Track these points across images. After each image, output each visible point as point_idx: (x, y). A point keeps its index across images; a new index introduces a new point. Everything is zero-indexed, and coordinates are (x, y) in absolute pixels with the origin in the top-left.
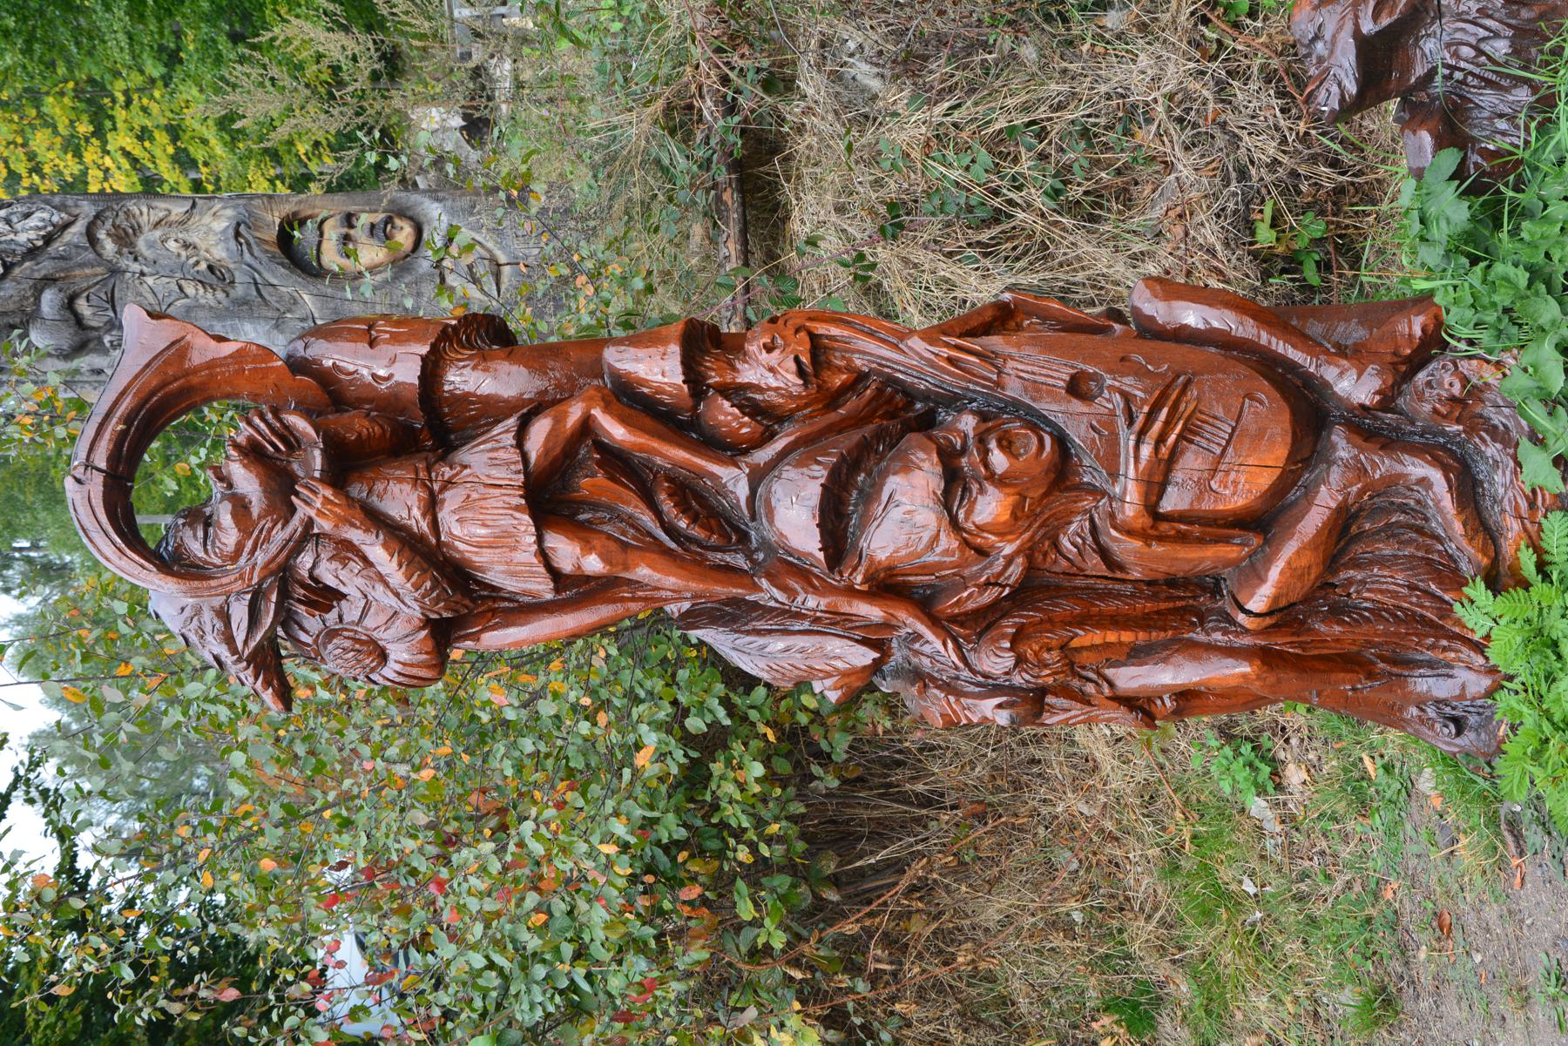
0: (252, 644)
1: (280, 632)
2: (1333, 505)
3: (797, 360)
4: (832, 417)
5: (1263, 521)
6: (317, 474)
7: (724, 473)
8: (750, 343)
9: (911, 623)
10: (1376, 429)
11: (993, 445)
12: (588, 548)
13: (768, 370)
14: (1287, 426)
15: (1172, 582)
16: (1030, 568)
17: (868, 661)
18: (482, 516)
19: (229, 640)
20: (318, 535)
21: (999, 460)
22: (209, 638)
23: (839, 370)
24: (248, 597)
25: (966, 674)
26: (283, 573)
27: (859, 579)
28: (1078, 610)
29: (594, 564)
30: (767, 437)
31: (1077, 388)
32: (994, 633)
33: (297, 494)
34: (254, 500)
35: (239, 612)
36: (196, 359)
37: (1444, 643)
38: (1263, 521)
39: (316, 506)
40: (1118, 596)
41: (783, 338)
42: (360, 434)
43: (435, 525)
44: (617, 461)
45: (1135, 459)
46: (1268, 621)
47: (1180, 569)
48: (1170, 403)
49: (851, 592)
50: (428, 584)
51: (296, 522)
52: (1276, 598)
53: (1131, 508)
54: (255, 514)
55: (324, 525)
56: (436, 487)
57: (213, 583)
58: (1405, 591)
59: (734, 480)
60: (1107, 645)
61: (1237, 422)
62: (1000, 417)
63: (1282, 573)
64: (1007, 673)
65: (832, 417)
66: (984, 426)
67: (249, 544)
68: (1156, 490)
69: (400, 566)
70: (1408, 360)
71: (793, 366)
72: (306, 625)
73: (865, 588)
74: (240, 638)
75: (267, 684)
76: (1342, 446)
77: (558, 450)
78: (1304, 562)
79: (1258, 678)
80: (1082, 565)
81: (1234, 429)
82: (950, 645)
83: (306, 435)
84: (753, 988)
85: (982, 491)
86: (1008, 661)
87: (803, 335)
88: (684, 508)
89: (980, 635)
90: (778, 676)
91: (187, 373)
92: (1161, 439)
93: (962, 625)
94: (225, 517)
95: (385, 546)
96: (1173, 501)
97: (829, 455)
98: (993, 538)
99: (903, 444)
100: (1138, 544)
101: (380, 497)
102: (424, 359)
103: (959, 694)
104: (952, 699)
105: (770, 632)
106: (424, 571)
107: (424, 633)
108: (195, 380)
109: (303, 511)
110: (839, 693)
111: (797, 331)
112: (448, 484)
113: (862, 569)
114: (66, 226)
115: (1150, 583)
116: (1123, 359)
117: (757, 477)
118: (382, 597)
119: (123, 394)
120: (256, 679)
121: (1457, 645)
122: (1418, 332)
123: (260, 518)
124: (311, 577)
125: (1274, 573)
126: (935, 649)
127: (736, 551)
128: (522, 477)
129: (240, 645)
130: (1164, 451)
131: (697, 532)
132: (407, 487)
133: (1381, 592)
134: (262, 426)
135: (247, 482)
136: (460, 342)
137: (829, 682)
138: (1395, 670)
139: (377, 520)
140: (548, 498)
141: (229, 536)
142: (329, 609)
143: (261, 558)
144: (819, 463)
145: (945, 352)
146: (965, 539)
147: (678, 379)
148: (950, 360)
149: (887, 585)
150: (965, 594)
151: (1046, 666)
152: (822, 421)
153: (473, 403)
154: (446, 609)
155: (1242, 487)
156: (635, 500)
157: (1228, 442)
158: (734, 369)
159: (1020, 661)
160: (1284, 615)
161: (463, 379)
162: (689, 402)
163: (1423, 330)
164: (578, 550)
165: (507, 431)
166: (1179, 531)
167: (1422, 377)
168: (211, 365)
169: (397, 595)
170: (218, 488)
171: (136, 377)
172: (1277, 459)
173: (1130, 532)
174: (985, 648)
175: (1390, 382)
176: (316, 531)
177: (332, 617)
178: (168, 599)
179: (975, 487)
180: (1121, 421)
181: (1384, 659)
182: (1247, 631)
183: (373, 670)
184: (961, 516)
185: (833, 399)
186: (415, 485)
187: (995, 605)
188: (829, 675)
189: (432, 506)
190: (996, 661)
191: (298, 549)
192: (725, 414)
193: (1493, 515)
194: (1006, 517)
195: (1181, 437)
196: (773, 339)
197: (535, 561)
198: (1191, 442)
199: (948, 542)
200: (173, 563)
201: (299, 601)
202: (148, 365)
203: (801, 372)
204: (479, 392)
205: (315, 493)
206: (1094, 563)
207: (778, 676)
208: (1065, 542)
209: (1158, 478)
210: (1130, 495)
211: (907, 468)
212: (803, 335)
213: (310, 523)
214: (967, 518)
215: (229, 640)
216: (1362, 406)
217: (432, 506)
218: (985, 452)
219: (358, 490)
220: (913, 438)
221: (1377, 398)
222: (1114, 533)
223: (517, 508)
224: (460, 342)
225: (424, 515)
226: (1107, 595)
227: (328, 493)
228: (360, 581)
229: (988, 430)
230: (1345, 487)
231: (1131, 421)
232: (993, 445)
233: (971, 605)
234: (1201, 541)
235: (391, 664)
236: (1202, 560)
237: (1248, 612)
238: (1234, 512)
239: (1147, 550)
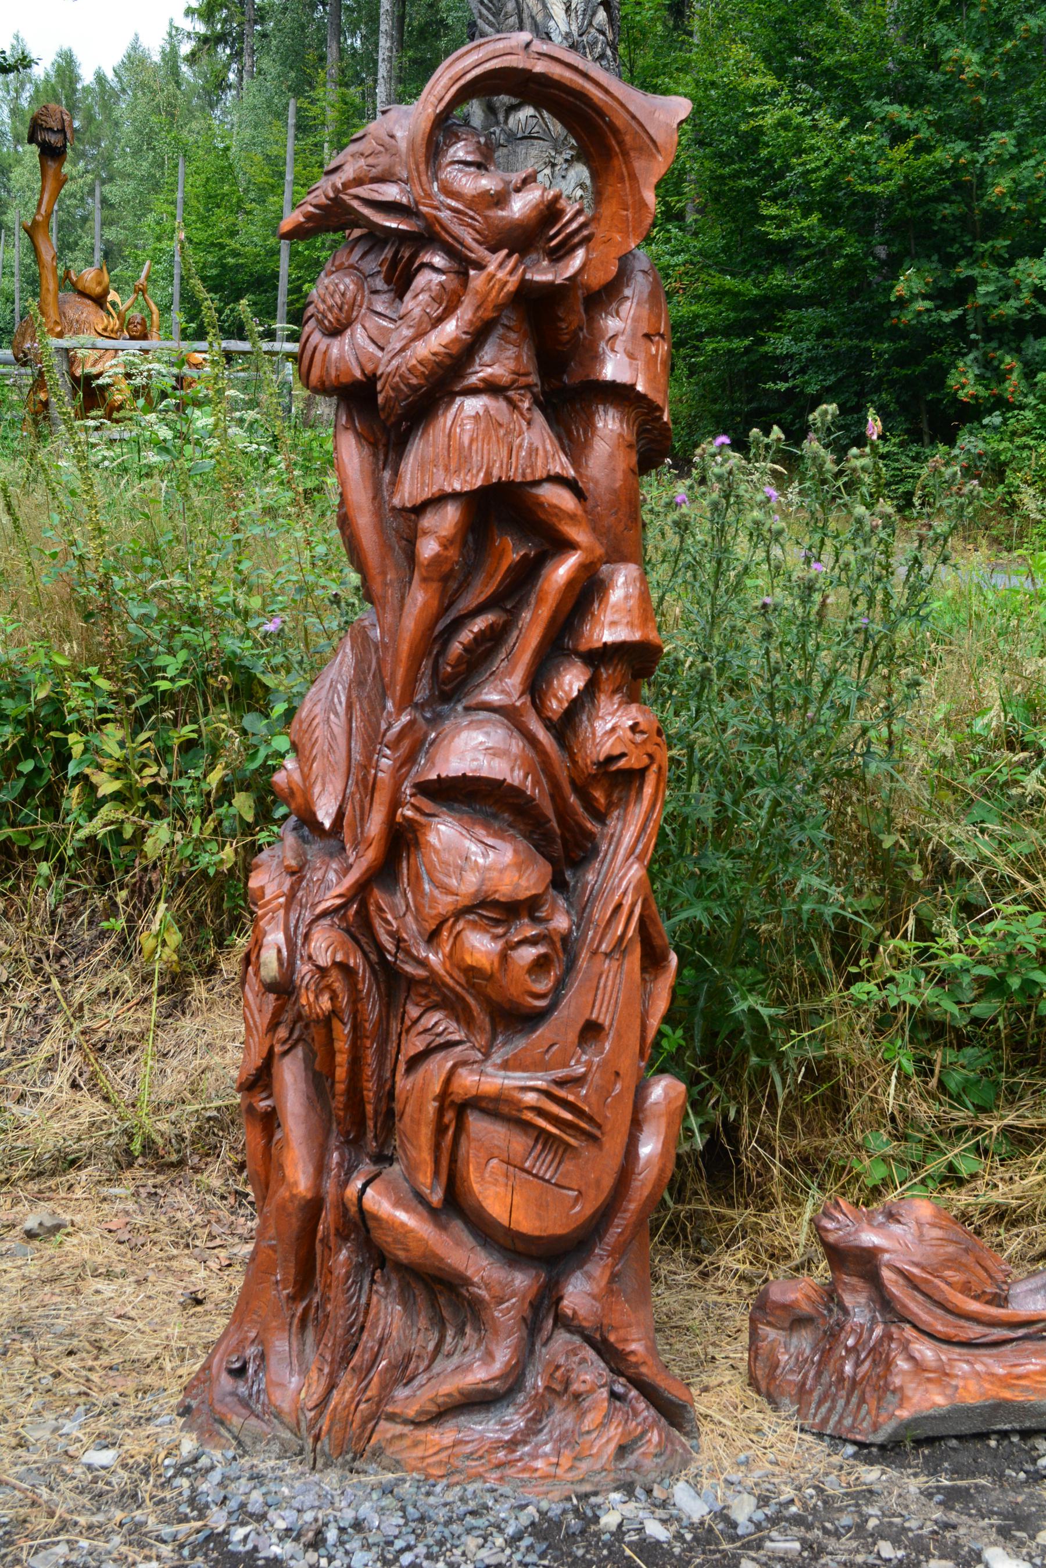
0: (355, 204)
1: (357, 233)
2: (469, 1273)
3: (623, 755)
4: (567, 788)
5: (455, 1205)
6: (528, 276)
7: (514, 681)
8: (639, 710)
9: (362, 861)
10: (544, 1311)
11: (541, 950)
12: (446, 544)
13: (612, 726)
14: (551, 1231)
15: (390, 1114)
16: (412, 982)
18: (478, 438)
19: (359, 182)
20: (466, 274)
21: (529, 953)
22: (362, 162)
23: (609, 796)
24: (405, 200)
25: (308, 916)
26: (430, 236)
27: (409, 813)
28: (369, 1026)
29: (428, 548)
30: (549, 725)
31: (591, 1031)
32: (351, 944)
33: (509, 256)
34: (501, 213)
35: (391, 192)
36: (639, 164)
37: (326, 1370)
38: (455, 1205)
39: (499, 273)
40: (381, 1064)
41: (644, 742)
42: (562, 320)
43: (473, 391)
44: (525, 577)
46: (353, 1209)
47: (404, 1124)
48: (576, 1121)
49: (395, 804)
50: (414, 381)
51: (480, 252)
52: (376, 1218)
53: (468, 1081)
54: (490, 213)
55: (477, 279)
56: (511, 393)
57: (422, 167)
58: (378, 1335)
59: (503, 687)
60: (331, 1053)
61: (556, 1185)
62: (562, 955)
63: (403, 1224)
64: (310, 957)
65: (567, 788)
66: (557, 939)
68: (491, 1106)
69: (434, 354)
70: (605, 1340)
71: (616, 752)
72: (370, 258)
73: (399, 819)
74: (362, 191)
75: (309, 217)
76: (521, 1281)
77: (543, 517)
78: (412, 1245)
79: (293, 1196)
80: (414, 1032)
81: (548, 1181)
82: (338, 901)
83: (567, 267)
85: (496, 938)
86: (324, 960)
87: (646, 760)
88: (480, 638)
89: (347, 931)
90: (305, 726)
91: (625, 154)
92: (540, 1112)
93: (357, 912)
94: (487, 183)
95: (456, 340)
97: (534, 786)
98: (447, 949)
99: (541, 859)
100: (437, 1089)
101: (502, 338)
102: (632, 387)
103: (288, 907)
104: (282, 900)
105: (350, 721)
106: (426, 378)
107: (358, 374)
109: (493, 261)
110: (284, 785)
111: (651, 756)
112: (513, 405)
113: (418, 817)
115: (391, 1095)
116: (617, 1074)
117: (508, 714)
118: (396, 336)
119: (607, 92)
120: (315, 206)
121: (324, 1381)
122: (633, 1346)
123: (486, 218)
124: (423, 265)
125: (402, 1216)
126: (332, 884)
127: (431, 689)
128: (519, 479)
129: (354, 191)
130: (529, 1116)
131: (456, 648)
132: (512, 364)
133: (377, 1313)
134: (574, 225)
135: (520, 206)
136: (646, 422)
137: (297, 777)
138: (296, 1321)
139: (479, 335)
140: (499, 508)
141: (472, 183)
142: (388, 280)
143: (445, 215)
144: (526, 777)
145: (627, 901)
146: (446, 920)
147: (608, 637)
148: (619, 906)
149: (401, 841)
150: (389, 917)
151: (317, 997)
152: (563, 776)
153: (585, 434)
154: (387, 399)
155: (494, 1195)
156: (489, 590)
157: (536, 1176)
158: (615, 692)
159: (322, 971)
160: (360, 1226)
161: (609, 424)
162: (583, 646)
163: (632, 1352)
164: (444, 533)
165: (563, 467)
166: (447, 1127)
167: (590, 1354)
169: (403, 349)
170: (516, 178)
171: (622, 105)
172: (518, 1222)
173: (448, 1081)
174: (337, 935)
175: (585, 1324)
176: (472, 272)
177: (379, 283)
178: (404, 123)
179: (500, 931)
180: (560, 1073)
181: (306, 1310)
182: (345, 1184)
183: (320, 322)
184: (471, 917)
185: (582, 792)
186: (514, 373)
187: (380, 949)
188: (305, 777)
189: (491, 388)
190: (324, 946)
191: (450, 252)
192: (572, 681)
193: (451, 1424)
194: (469, 960)
195: (542, 1131)
196: (642, 732)
197: (435, 489)
198: (536, 1141)
199: (445, 903)
200: (444, 127)
201: (397, 252)
202: (634, 117)
203: (611, 759)
204: (596, 439)
205: (511, 273)
206: (416, 1044)
207: (305, 726)
208: (436, 1016)
209: (505, 1109)
211: (519, 866)
212: (646, 760)
213: (480, 266)
214: (468, 921)
215: (359, 182)
216: (561, 1298)
217: (491, 388)
218: (532, 941)
219: (509, 318)
220: (547, 869)
221: (569, 1312)
222: (450, 1064)
223: (488, 474)
224: (646, 422)
225: (483, 380)
226: (381, 1054)
227: (510, 287)
228: (417, 312)
229: (552, 943)
230: (487, 1285)
231: (561, 1083)
232: (541, 950)
233: (377, 922)
234: (437, 1147)
235: (326, 341)
236: (419, 1148)
237: (363, 1191)
238: (466, 1180)
239: (431, 1096)
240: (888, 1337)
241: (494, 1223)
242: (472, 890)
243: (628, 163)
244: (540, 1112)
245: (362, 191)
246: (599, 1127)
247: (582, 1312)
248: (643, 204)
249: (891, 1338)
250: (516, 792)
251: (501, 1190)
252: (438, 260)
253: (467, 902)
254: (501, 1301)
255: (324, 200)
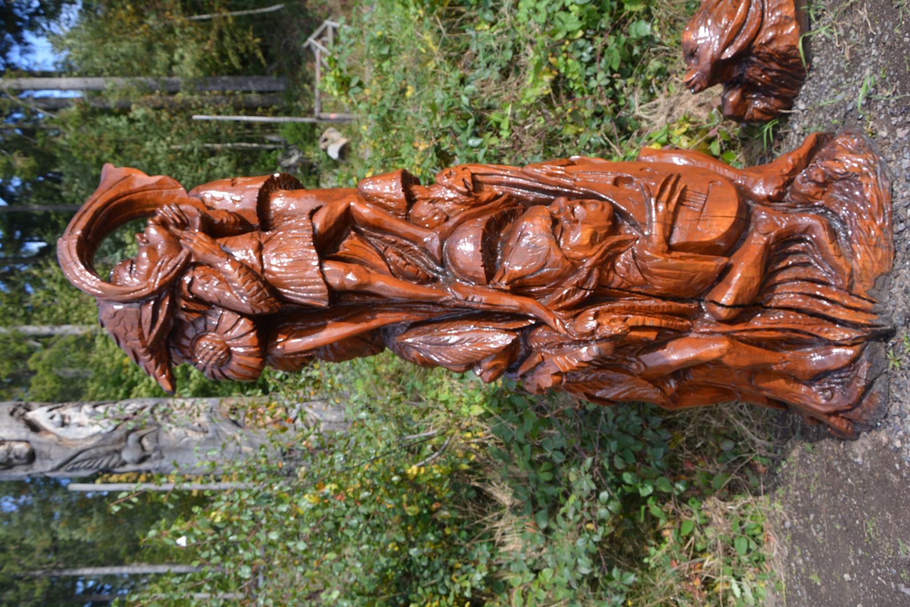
0: (155, 332)
17: (509, 342)
27: (504, 282)
36: (137, 185)
43: (261, 259)
45: (657, 211)
50: (255, 288)
52: (738, 296)
54: (160, 253)
67: (156, 269)
73: (508, 288)
77: (332, 224)
84: (580, 108)
91: (131, 193)
92: (668, 201)
96: (674, 241)
108: (135, 197)
114: (142, 409)
130: (671, 208)
155: (717, 226)
168: (144, 189)
184: (562, 242)
191: (182, 272)
194: (587, 241)
209: (669, 222)
210: (655, 231)
223: (309, 247)
225: (255, 253)
240: (757, 55)
241: (734, 225)
242: (546, 239)
243: (136, 192)
244: (668, 201)
245: (146, 328)
246: (671, 175)
247: (776, 185)
248: (159, 183)
249: (758, 53)
250: (488, 224)
251: (714, 223)
252: (187, 279)
253: (554, 243)
254: (776, 225)
255: (153, 362)
